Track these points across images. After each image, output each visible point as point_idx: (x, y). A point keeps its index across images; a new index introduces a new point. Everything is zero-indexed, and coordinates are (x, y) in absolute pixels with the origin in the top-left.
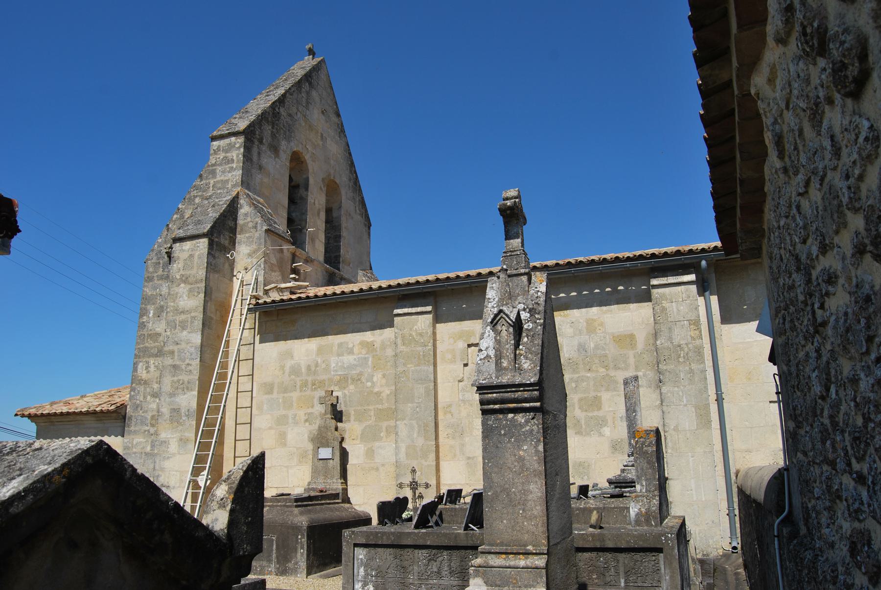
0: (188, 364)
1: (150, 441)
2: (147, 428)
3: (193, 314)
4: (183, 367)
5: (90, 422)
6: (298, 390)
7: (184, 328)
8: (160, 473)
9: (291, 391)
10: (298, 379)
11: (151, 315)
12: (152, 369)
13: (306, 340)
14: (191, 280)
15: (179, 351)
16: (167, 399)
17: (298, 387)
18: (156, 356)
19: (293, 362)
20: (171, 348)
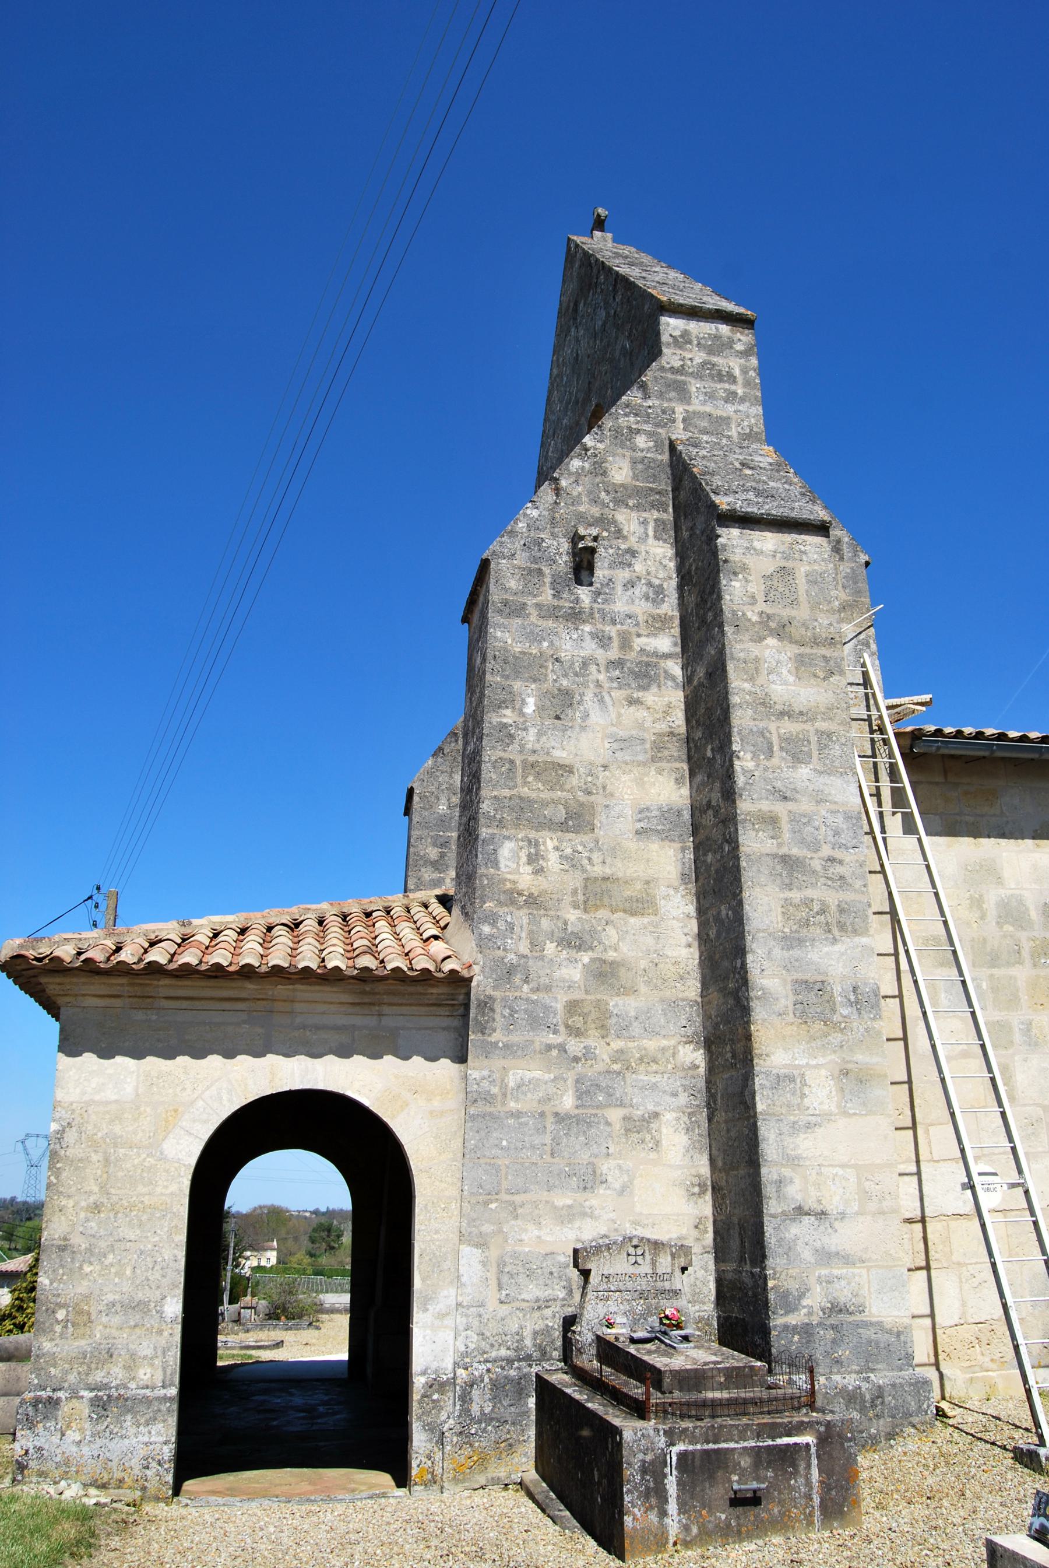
0: (832, 860)
1: (571, 1076)
2: (552, 1039)
3: (822, 725)
4: (817, 865)
5: (327, 1008)
6: (1028, 961)
7: (798, 758)
8: (787, 1172)
9: (1009, 964)
10: (1023, 936)
11: (530, 708)
12: (553, 862)
13: (1029, 842)
14: (796, 632)
15: (794, 818)
16: (777, 952)
17: (1026, 954)
18: (563, 827)
19: (1003, 892)
20: (765, 806)
